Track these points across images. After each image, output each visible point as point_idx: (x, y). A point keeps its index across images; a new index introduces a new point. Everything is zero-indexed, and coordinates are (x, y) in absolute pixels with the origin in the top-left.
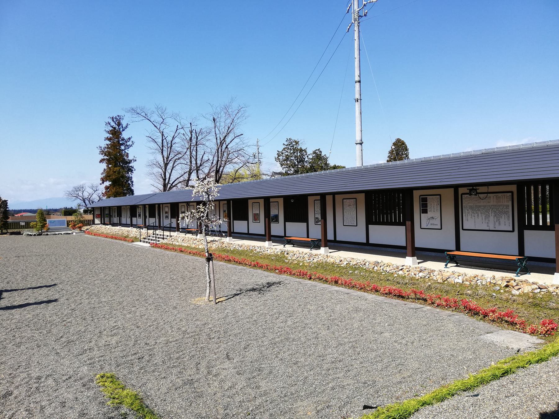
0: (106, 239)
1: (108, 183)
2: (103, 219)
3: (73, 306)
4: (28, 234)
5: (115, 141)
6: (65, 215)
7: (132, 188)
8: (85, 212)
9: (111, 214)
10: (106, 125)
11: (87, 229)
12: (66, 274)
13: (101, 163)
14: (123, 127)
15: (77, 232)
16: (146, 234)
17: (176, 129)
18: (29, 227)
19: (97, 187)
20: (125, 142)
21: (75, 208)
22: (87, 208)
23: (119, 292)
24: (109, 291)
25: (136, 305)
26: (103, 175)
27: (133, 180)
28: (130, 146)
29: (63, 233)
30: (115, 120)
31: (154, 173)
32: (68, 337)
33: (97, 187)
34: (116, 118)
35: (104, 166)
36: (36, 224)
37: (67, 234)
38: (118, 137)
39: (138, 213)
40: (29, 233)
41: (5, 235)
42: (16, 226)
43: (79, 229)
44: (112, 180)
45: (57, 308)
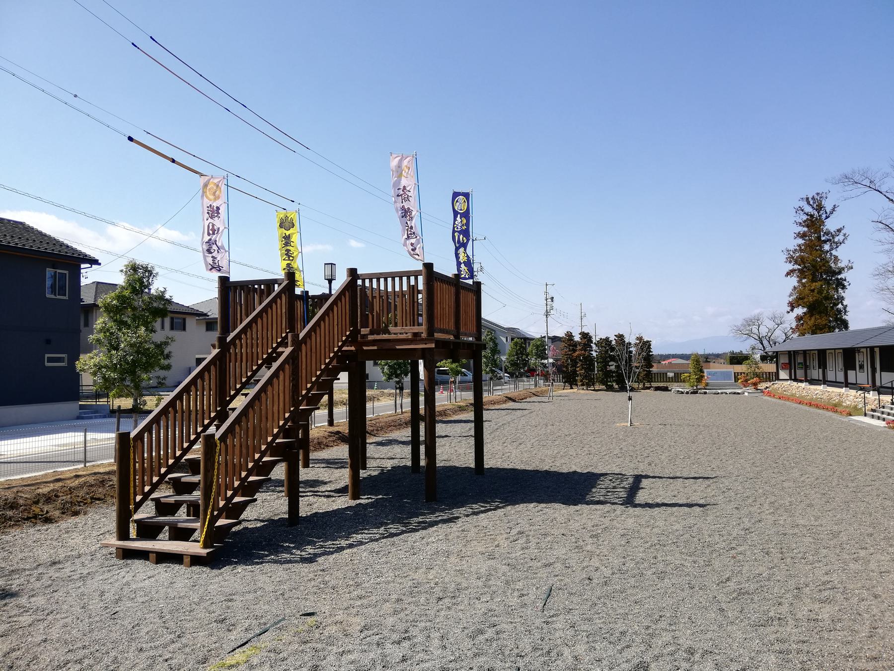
0: (800, 406)
1: (800, 311)
2: (793, 371)
3: (747, 525)
4: (678, 391)
5: (813, 238)
6: (731, 363)
7: (844, 317)
8: (764, 358)
9: (808, 364)
10: (796, 212)
11: (767, 387)
12: (735, 462)
13: (787, 276)
14: (826, 213)
15: (750, 391)
16: (877, 402)
18: (680, 380)
19: (781, 318)
20: (831, 238)
21: (747, 353)
22: (766, 353)
23: (829, 511)
24: (810, 505)
25: (867, 546)
26: (792, 297)
28: (841, 243)
29: (728, 391)
31: (889, 287)
32: (739, 583)
33: (781, 318)
35: (794, 281)
36: (689, 376)
37: (734, 393)
38: (818, 230)
39: (859, 361)
40: (680, 390)
41: (648, 391)
42: (659, 379)
43: (753, 387)
44: (807, 305)
45: (721, 522)
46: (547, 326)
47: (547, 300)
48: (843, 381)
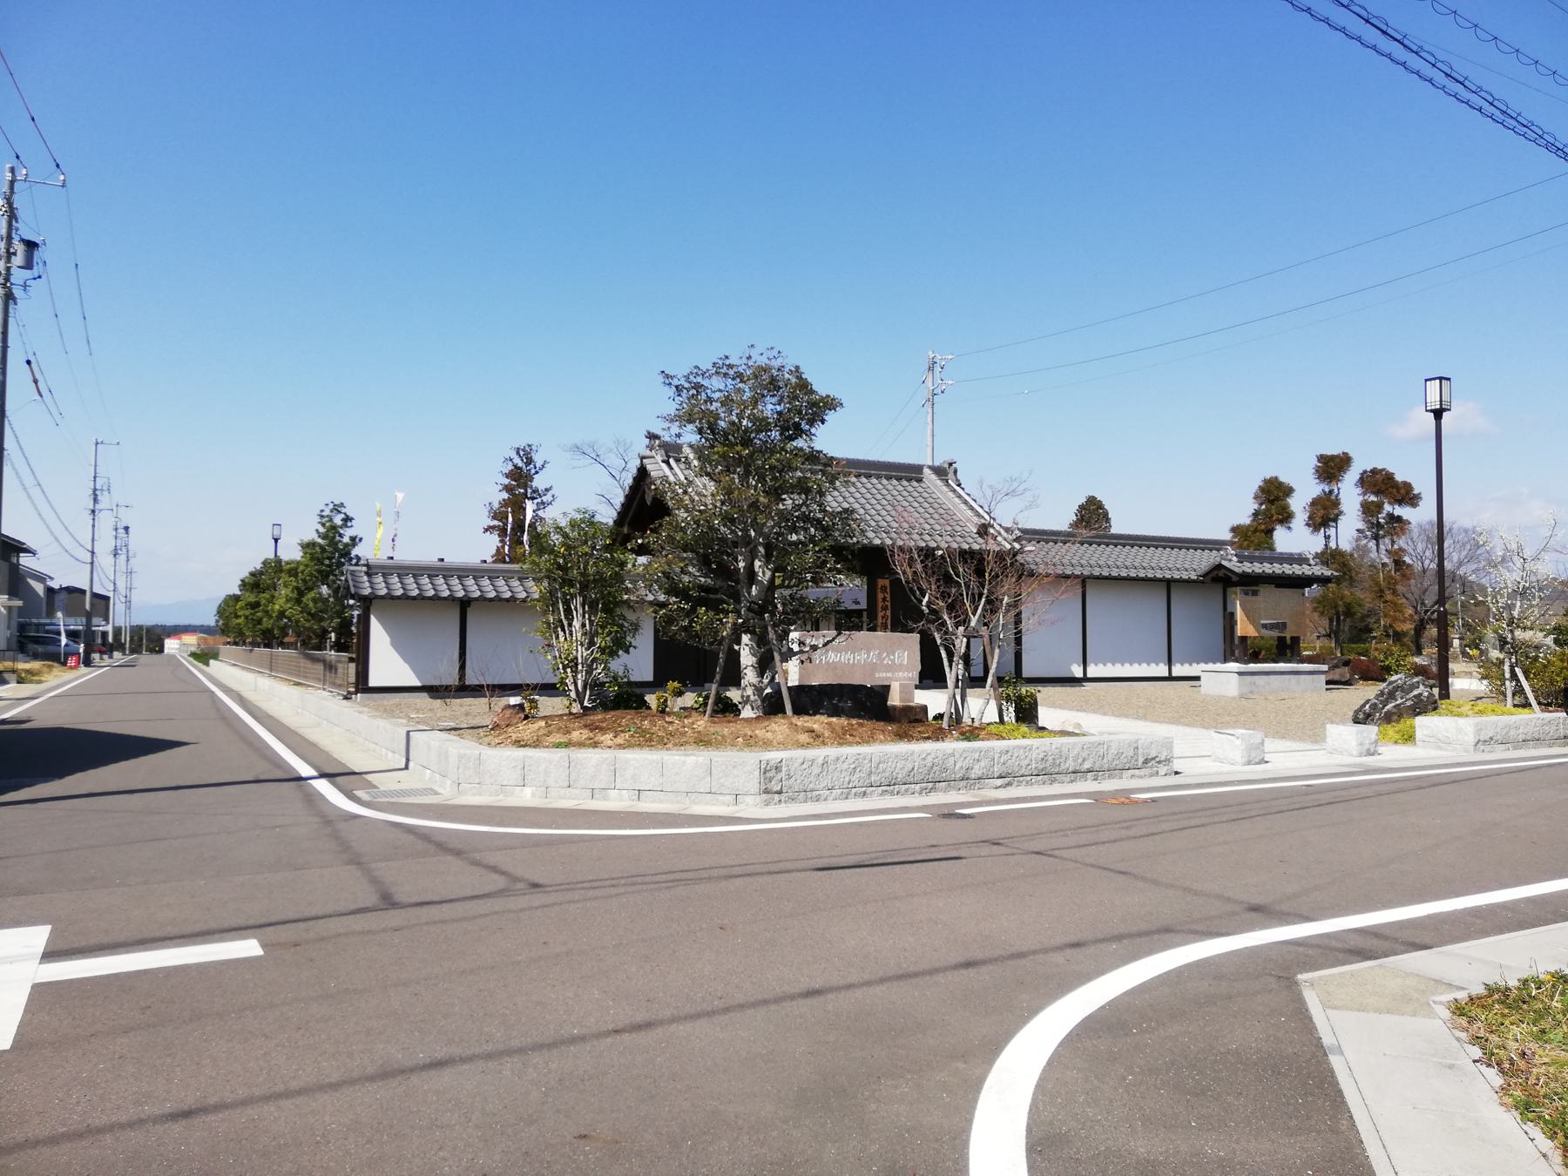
14: (535, 468)
34: (523, 450)
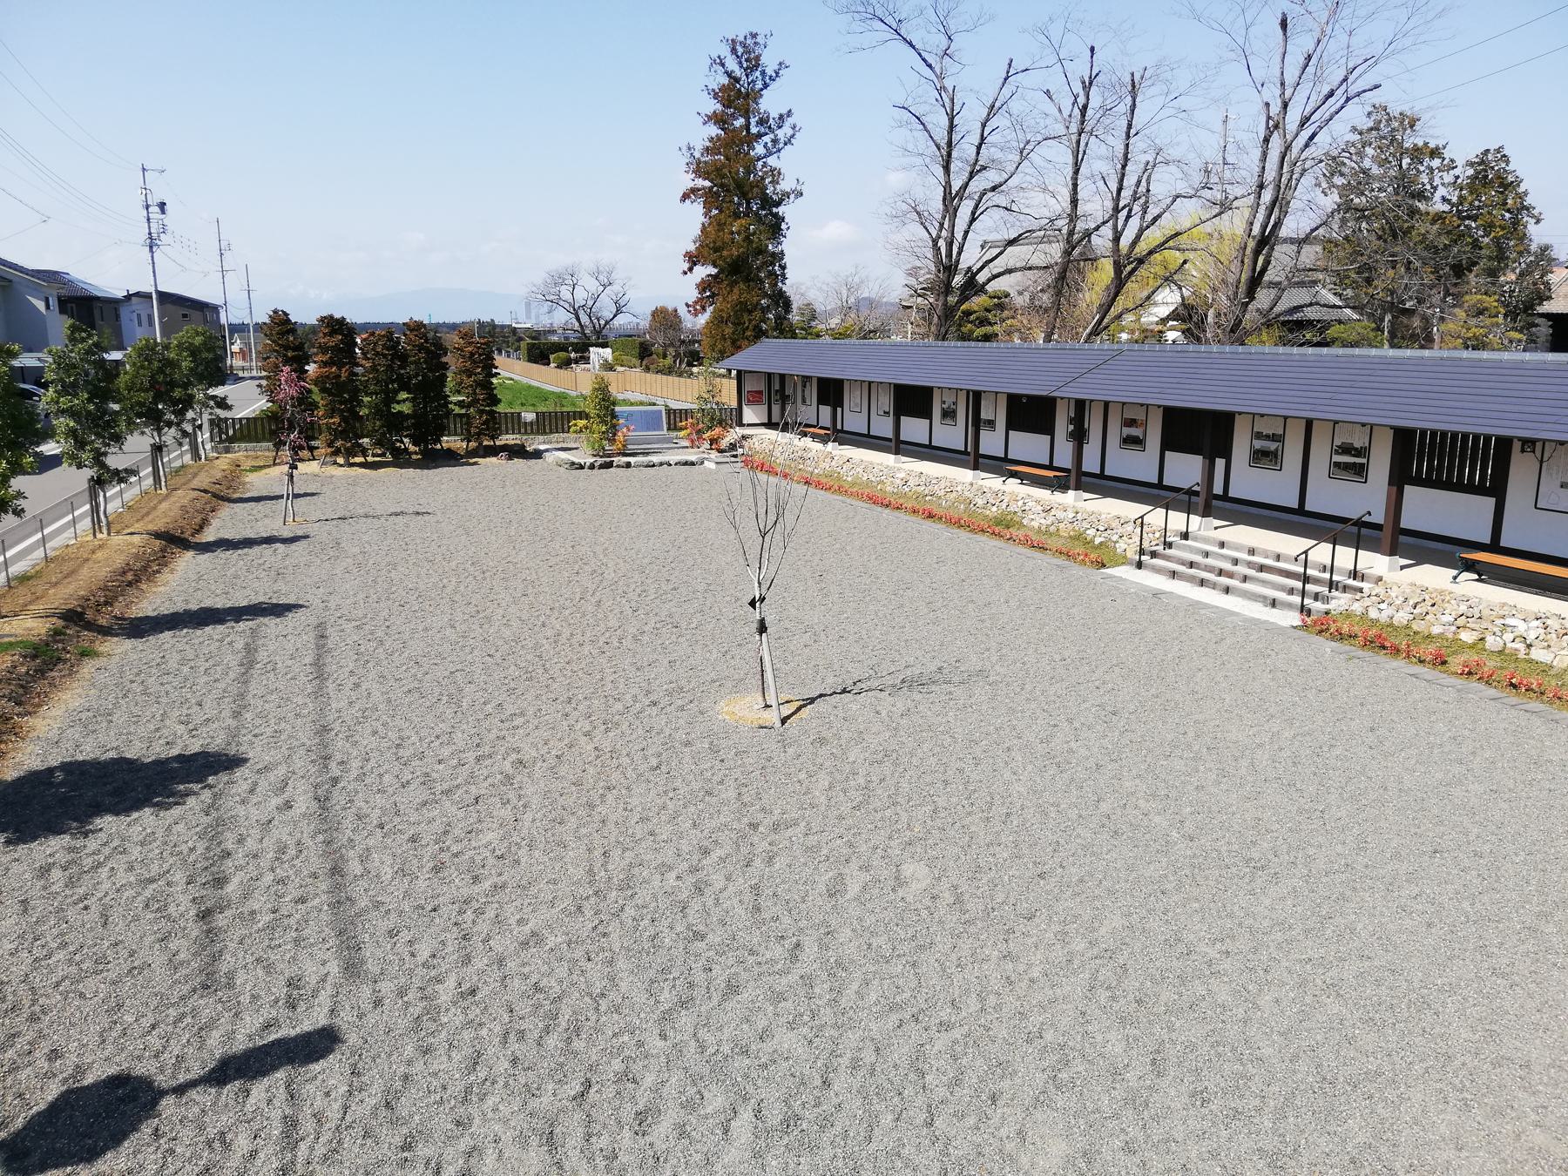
1: (703, 271)
4: (573, 463)
17: (1004, 75)
19: (610, 273)
27: (786, 260)
30: (740, 50)
37: (686, 463)
41: (494, 460)
46: (154, 272)
47: (147, 207)
48: (890, 435)
